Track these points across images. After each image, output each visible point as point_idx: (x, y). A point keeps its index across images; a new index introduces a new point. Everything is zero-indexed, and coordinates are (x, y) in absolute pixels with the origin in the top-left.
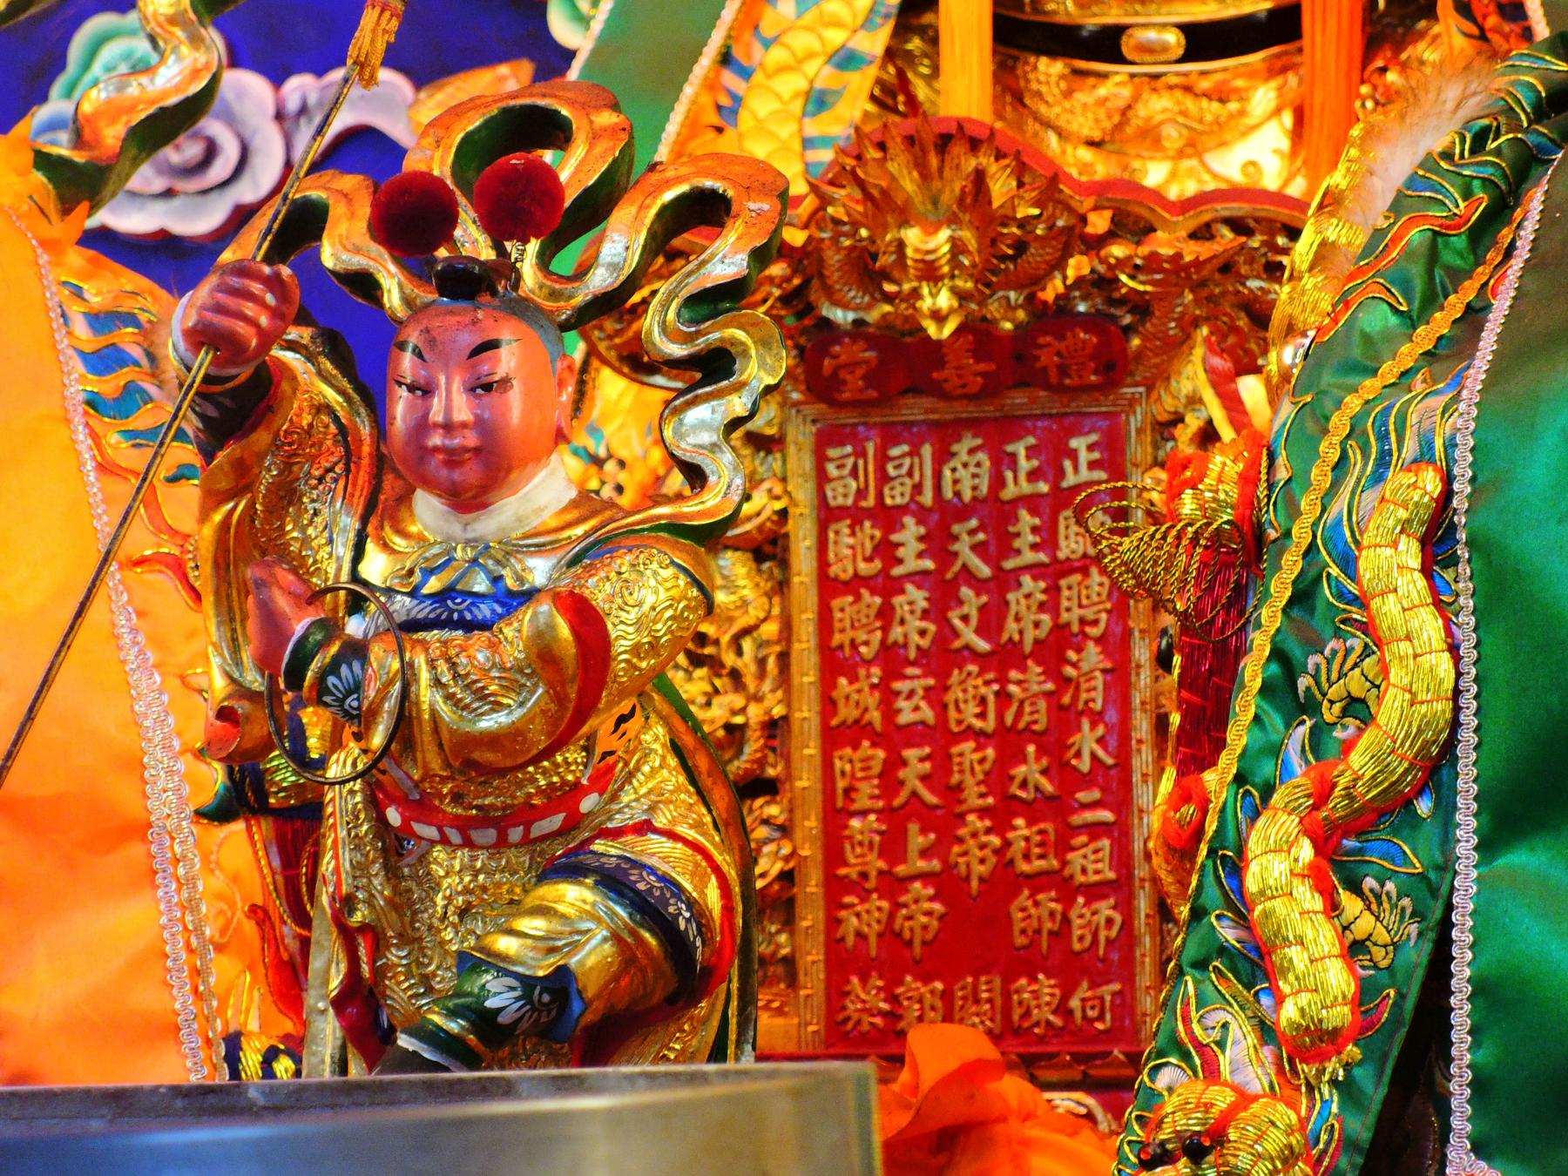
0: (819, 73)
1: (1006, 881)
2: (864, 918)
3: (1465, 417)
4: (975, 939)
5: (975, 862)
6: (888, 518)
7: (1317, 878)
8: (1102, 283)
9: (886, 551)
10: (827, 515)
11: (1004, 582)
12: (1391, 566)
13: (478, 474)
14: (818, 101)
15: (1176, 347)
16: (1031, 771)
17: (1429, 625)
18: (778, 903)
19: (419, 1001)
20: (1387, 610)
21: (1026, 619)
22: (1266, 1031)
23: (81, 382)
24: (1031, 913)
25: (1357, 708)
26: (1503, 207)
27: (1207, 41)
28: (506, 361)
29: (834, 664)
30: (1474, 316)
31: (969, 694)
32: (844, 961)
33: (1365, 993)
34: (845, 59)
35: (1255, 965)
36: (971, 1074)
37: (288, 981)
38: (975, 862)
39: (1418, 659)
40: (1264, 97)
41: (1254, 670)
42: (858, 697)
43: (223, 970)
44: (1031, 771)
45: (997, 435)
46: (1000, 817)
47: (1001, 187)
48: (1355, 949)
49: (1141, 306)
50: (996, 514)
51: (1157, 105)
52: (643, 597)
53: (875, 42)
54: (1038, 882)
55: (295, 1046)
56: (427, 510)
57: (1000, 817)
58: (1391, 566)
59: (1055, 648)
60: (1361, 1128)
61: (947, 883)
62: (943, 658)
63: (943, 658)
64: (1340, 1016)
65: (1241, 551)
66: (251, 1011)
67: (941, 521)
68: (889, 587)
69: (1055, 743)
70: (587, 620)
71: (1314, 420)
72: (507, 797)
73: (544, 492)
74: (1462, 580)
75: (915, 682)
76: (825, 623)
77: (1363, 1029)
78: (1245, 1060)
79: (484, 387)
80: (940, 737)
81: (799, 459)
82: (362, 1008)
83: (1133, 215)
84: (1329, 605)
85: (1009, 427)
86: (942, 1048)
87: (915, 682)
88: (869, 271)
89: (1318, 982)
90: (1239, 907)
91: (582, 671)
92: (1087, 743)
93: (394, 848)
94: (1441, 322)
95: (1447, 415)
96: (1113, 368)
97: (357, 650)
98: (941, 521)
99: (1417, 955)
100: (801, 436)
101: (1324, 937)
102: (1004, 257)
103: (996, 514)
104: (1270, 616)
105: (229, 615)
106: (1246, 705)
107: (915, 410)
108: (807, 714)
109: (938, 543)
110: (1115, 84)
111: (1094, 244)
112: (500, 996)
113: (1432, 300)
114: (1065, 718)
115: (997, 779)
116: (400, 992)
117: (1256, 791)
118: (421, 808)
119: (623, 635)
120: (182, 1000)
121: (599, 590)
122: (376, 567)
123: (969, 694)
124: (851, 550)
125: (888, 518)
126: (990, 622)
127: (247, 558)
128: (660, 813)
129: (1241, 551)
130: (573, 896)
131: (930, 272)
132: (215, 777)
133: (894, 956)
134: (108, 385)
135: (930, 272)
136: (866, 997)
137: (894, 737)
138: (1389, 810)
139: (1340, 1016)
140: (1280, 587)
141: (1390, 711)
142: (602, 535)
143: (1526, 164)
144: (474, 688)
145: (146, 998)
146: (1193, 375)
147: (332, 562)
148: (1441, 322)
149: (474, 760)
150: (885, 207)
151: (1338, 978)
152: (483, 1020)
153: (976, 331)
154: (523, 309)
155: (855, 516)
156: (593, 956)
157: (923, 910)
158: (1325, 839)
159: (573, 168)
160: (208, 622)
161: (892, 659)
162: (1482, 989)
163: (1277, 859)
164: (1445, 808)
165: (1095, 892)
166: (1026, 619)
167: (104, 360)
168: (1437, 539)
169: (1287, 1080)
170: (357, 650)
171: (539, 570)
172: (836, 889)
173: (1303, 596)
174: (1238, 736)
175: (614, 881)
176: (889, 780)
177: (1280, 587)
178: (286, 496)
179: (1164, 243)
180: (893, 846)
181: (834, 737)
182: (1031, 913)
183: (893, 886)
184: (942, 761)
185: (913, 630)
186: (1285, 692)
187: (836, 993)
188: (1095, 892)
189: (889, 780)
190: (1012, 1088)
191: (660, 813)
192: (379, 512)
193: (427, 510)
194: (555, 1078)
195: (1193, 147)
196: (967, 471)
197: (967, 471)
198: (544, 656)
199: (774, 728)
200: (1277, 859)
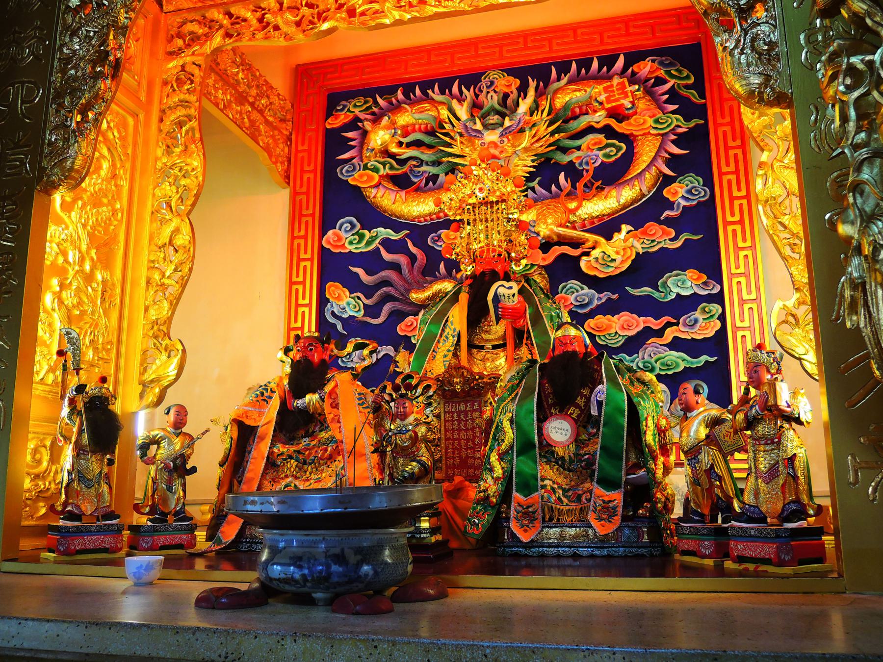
0: (446, 352)
1: (467, 457)
2: (450, 462)
3: (514, 407)
4: (464, 464)
5: (463, 455)
6: (453, 413)
7: (498, 460)
8: (478, 385)
9: (452, 417)
10: (445, 412)
11: (467, 421)
12: (506, 424)
13: (404, 416)
14: (445, 356)
15: (487, 392)
16: (470, 444)
17: (511, 431)
18: (440, 460)
19: (398, 476)
20: (506, 429)
21: (469, 426)
22: (493, 478)
23: (357, 402)
24: (471, 461)
25: (503, 441)
26: (521, 381)
27: (495, 347)
28: (407, 405)
29: (446, 431)
30: (517, 394)
31: (463, 435)
32: (447, 467)
33: (504, 473)
34: (449, 351)
35: (491, 470)
36: (461, 482)
37: (382, 471)
38: (463, 455)
39: (510, 434)
40: (502, 354)
41: (491, 436)
42: (449, 434)
43: (374, 471)
44: (470, 444)
45: (466, 402)
46: (466, 450)
47: (465, 374)
48: (502, 468)
49: (483, 387)
50: (466, 412)
51: (488, 355)
52: (422, 430)
53: (452, 349)
54: (471, 457)
55: (383, 479)
56: (398, 421)
57: (466, 450)
58: (506, 424)
59: (473, 429)
60: (503, 489)
61: (460, 458)
62: (459, 430)
63: (459, 430)
64: (501, 476)
65: (490, 422)
66: (377, 476)
67: (459, 413)
68: (453, 421)
69: (473, 441)
70: (416, 433)
71: (498, 407)
72: (409, 453)
73: (411, 419)
74: (514, 426)
75: (456, 433)
76: (445, 426)
77: (504, 477)
78: (490, 481)
79: (404, 408)
80: (459, 439)
81: (442, 406)
82: (391, 476)
83: (482, 376)
84: (500, 429)
85: (467, 402)
86: (458, 479)
87: (456, 433)
88: (451, 383)
89: (498, 472)
90: (490, 463)
91: (415, 439)
92: (477, 440)
93: (395, 458)
94: (513, 395)
95: (513, 407)
96: (480, 395)
97: (391, 437)
98: (459, 413)
99: (510, 469)
100: (442, 402)
101: (499, 467)
102: (466, 381)
103: (466, 412)
104: (493, 430)
105: (376, 431)
106: (490, 441)
107: (456, 399)
108: (443, 437)
109: (459, 416)
110: (483, 353)
111: (477, 380)
112: (406, 475)
113: (512, 393)
114: (474, 437)
115: (466, 445)
116: (395, 474)
117: (491, 450)
118: (397, 454)
119: (420, 435)
120: (369, 475)
121: (417, 430)
122: (392, 427)
123: (463, 435)
124: (448, 417)
125: (453, 413)
126: (465, 425)
127: (378, 427)
128: (424, 455)
129: (490, 422)
130: (414, 464)
131: (457, 384)
132: (373, 449)
133: (454, 467)
134: (360, 402)
135: (457, 384)
136: (450, 472)
137: (454, 440)
138: (506, 452)
139: (501, 476)
140: (494, 427)
141: (506, 441)
142: (418, 423)
143: (523, 376)
144: (403, 441)
145: (366, 474)
146: (489, 396)
147: (387, 426)
148: (513, 395)
149: (404, 449)
150: (452, 376)
151: (501, 471)
152: (404, 477)
153: (463, 390)
154: (409, 399)
155: (449, 412)
156: (416, 470)
157: (457, 461)
158: (499, 455)
159: (414, 382)
160: (372, 430)
161: (453, 430)
162: (516, 473)
163: (494, 458)
164: (513, 452)
165: (478, 459)
166: (469, 426)
167: (359, 399)
168: (511, 421)
169: (495, 484)
170: (391, 437)
171: (410, 427)
172: (447, 458)
173: (497, 427)
174: (489, 444)
175: (419, 462)
176: (453, 445)
177: (494, 427)
178: (382, 419)
179: (485, 380)
180: (453, 453)
181: (446, 440)
182: (471, 461)
183: (454, 458)
184: (459, 443)
185: (456, 427)
186: (494, 439)
187: (447, 471)
188: (478, 459)
189: (453, 445)
190: (467, 483)
191: (424, 455)
192: (393, 421)
193: (398, 421)
194: (137, 220)
195: (493, 361)
196: (462, 407)
197: (462, 407)
198: (411, 437)
199: (439, 439)
200: (494, 458)
